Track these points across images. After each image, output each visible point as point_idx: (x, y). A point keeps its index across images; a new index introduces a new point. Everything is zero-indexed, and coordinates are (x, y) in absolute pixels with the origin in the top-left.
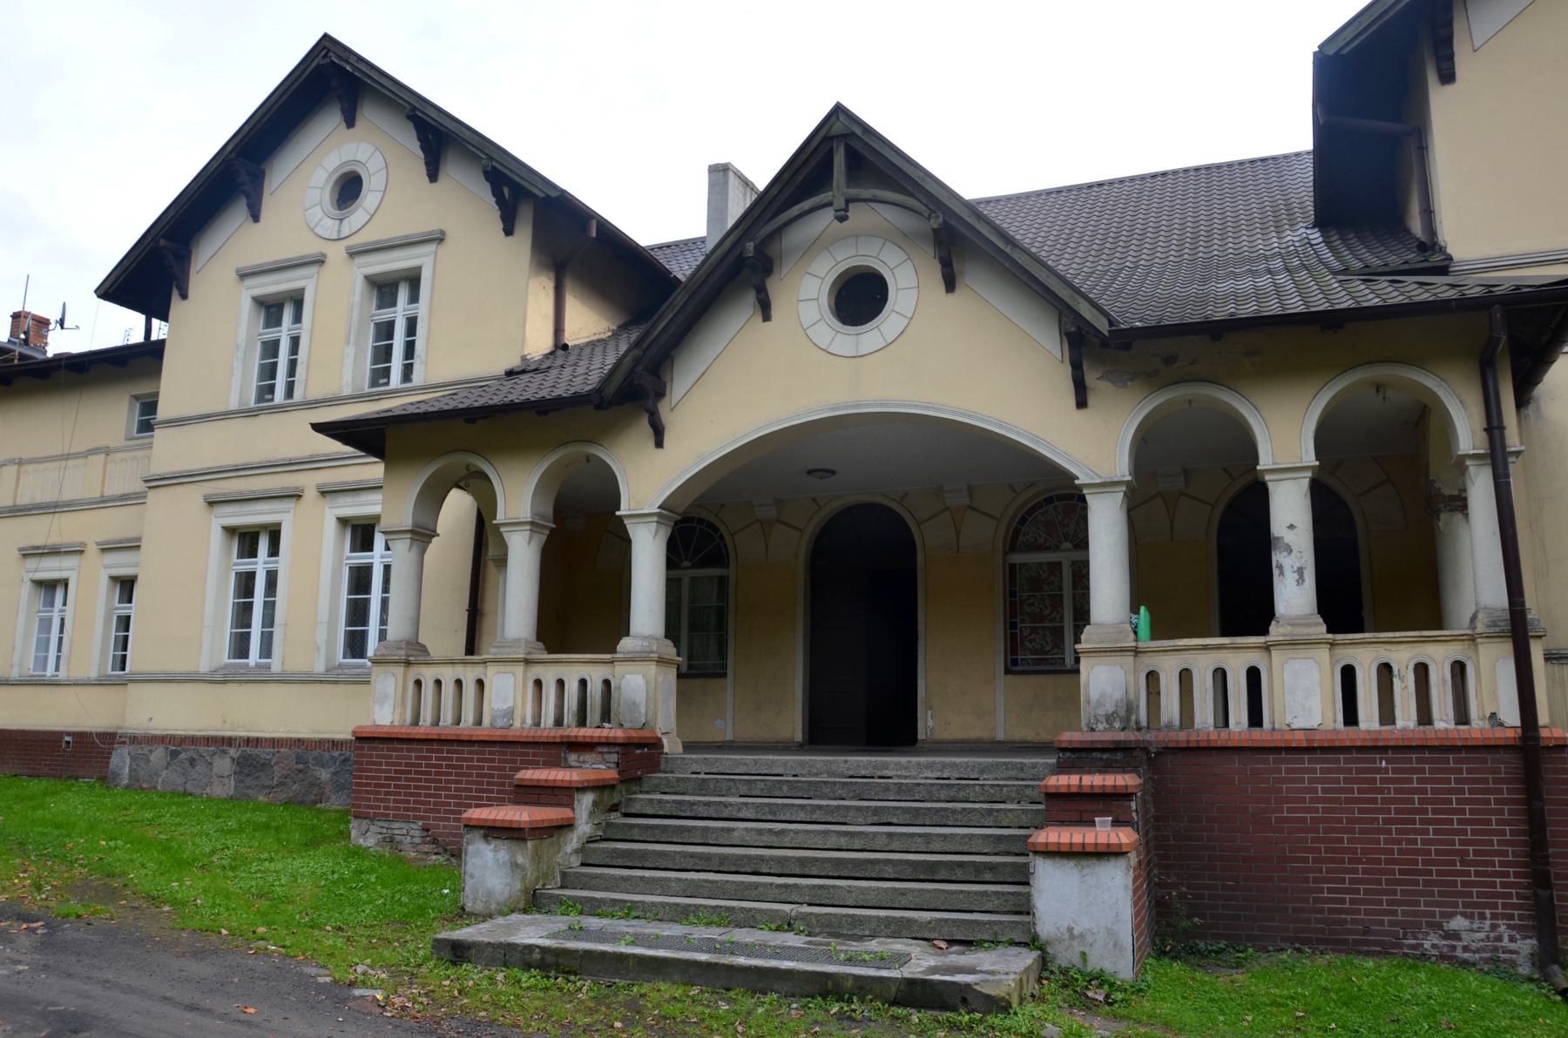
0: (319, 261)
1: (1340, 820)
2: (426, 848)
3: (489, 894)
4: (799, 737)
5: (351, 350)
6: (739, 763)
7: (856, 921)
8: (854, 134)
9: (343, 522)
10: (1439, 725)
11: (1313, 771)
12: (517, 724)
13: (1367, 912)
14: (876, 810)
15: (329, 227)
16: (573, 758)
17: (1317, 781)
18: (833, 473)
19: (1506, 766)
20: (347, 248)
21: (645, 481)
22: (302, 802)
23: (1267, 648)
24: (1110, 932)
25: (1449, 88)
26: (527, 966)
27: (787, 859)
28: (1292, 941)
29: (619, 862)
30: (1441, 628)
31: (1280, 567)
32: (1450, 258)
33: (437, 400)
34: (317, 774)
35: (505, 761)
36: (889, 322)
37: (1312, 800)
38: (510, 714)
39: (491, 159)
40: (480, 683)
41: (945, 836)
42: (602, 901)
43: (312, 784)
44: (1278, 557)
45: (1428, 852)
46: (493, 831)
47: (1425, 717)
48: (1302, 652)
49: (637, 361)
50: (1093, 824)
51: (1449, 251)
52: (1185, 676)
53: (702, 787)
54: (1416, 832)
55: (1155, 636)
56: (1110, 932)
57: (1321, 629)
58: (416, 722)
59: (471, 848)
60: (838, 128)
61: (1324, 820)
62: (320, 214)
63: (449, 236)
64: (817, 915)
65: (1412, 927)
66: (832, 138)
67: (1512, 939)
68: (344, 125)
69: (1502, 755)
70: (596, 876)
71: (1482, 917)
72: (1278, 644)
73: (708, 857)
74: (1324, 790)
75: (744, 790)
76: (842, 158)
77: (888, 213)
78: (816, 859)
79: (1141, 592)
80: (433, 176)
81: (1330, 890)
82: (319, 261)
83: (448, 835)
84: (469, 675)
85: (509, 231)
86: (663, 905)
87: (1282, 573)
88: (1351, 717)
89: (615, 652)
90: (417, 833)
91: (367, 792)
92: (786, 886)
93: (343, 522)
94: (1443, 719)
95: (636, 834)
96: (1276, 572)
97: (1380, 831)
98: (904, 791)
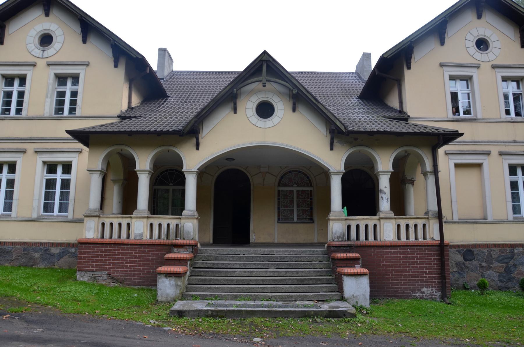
0: (34, 65)
1: (398, 265)
2: (109, 281)
3: (168, 295)
4: (211, 241)
5: (48, 100)
6: (226, 251)
7: (290, 297)
8: (269, 61)
9: (44, 163)
10: (411, 239)
11: (391, 252)
12: (144, 238)
13: (404, 288)
14: (278, 265)
15: (38, 52)
16: (175, 250)
17: (393, 254)
18: (234, 159)
19: (435, 250)
20: (47, 62)
21: (193, 160)
22: (26, 266)
23: (379, 219)
24: (364, 295)
25: (409, 71)
26: (207, 316)
27: (258, 280)
28: (386, 296)
29: (202, 283)
30: (404, 215)
31: (382, 198)
32: (409, 116)
33: (110, 124)
34: (34, 255)
35: (141, 251)
36: (275, 119)
37: (391, 259)
38: (142, 235)
39: (114, 40)
40: (129, 225)
41: (302, 271)
42: (207, 295)
43: (31, 259)
44: (380, 195)
45: (418, 272)
46: (168, 275)
47: (416, 238)
48: (388, 221)
49: (196, 122)
50: (355, 267)
51: (408, 114)
52: (358, 227)
53: (216, 259)
54: (415, 267)
55: (348, 215)
56: (364, 295)
57: (392, 215)
58: (103, 236)
59: (160, 280)
60: (265, 58)
61: (394, 265)
62: (34, 47)
63: (91, 64)
64: (278, 296)
65: (414, 291)
66: (262, 61)
67: (436, 292)
68: (44, 15)
69: (435, 247)
70: (199, 288)
71: (429, 287)
72: (383, 218)
73: (232, 280)
74: (394, 257)
75: (231, 259)
76: (265, 66)
77: (276, 86)
78: (268, 280)
79: (345, 203)
80: (84, 42)
81: (395, 283)
82: (34, 65)
83: (118, 276)
84: (124, 222)
85: (116, 66)
86: (228, 295)
87: (383, 199)
88: (399, 238)
89: (181, 215)
90: (105, 276)
91: (84, 262)
92: (263, 288)
93: (44, 163)
94: (421, 239)
95: (202, 274)
96: (380, 199)
97: (407, 267)
98: (282, 259)
